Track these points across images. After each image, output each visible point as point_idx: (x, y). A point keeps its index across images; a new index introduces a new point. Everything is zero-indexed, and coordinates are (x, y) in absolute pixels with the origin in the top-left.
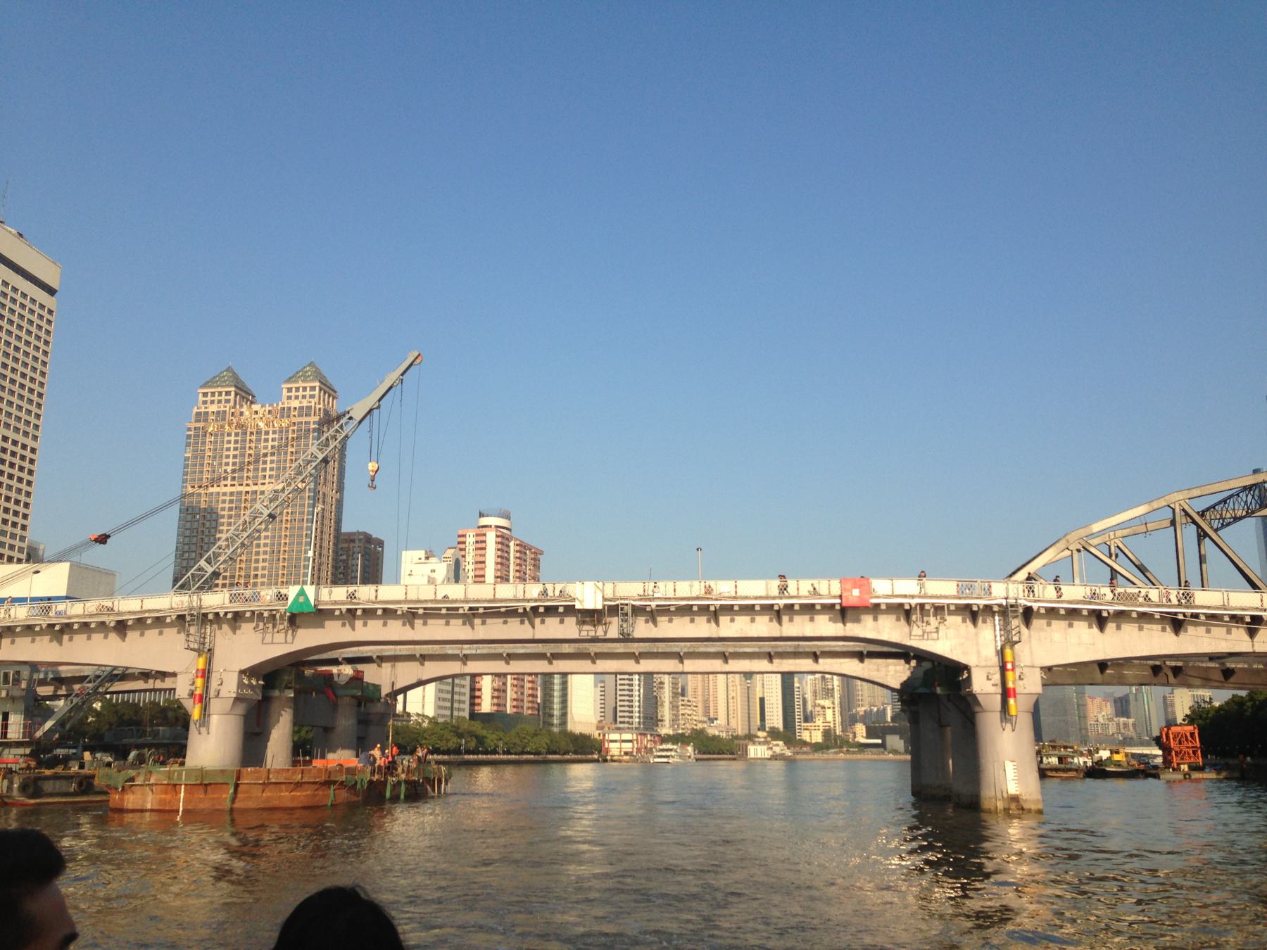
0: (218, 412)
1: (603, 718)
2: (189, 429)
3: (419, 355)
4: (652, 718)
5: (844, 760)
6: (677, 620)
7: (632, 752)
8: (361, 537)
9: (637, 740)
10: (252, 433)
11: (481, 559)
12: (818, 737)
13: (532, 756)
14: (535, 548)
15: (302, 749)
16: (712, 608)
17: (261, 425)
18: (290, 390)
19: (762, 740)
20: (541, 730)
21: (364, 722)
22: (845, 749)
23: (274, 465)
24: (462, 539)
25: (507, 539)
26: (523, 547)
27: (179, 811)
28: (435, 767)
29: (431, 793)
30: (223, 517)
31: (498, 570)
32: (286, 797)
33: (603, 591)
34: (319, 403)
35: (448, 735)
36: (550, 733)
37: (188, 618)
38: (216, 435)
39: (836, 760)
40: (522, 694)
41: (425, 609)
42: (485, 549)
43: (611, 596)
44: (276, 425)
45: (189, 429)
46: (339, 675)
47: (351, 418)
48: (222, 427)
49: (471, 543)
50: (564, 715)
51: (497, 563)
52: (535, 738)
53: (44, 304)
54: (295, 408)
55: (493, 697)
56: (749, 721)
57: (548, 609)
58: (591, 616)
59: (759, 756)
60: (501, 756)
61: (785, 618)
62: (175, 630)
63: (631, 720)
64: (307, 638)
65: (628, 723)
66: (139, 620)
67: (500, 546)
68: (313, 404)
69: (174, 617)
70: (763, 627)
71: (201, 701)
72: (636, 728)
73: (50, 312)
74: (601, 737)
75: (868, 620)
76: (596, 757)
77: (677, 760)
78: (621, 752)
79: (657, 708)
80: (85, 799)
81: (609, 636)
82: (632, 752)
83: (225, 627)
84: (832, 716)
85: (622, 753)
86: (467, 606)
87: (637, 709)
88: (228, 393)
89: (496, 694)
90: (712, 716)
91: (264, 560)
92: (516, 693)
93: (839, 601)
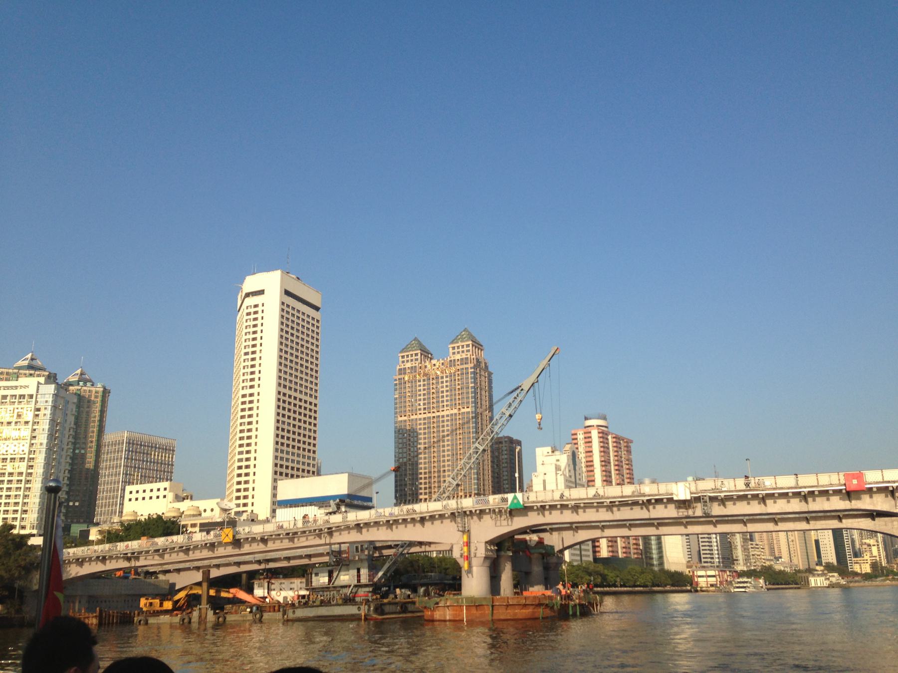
0: (412, 367)
1: (690, 559)
2: (396, 380)
3: (558, 349)
4: (729, 559)
5: (892, 585)
6: (738, 504)
7: (716, 584)
8: (506, 440)
9: (719, 575)
10: (433, 379)
11: (589, 449)
12: (867, 569)
13: (642, 588)
14: (626, 439)
15: (520, 584)
16: (761, 496)
17: (439, 373)
18: (454, 348)
19: (821, 572)
20: (645, 569)
21: (546, 568)
22: (891, 577)
23: (449, 398)
24: (574, 437)
25: (606, 434)
26: (618, 439)
27: (463, 621)
28: (593, 595)
29: (593, 612)
30: (421, 434)
31: (602, 456)
32: (510, 613)
33: (690, 488)
34: (473, 355)
35: (581, 574)
36: (653, 571)
37: (457, 514)
38: (412, 382)
39: (883, 586)
40: (629, 543)
41: (584, 503)
42: (591, 442)
43: (695, 491)
44: (447, 372)
45: (396, 380)
46: (530, 541)
47: (522, 390)
48: (415, 376)
49: (581, 439)
50: (661, 558)
51: (601, 452)
52: (643, 575)
53: (309, 314)
54: (458, 360)
55: (608, 546)
56: (808, 559)
57: (657, 500)
58: (683, 504)
59: (819, 585)
60: (620, 589)
61: (810, 500)
62: (449, 520)
63: (712, 560)
64: (520, 522)
65: (710, 562)
66: (431, 516)
67: (601, 440)
68: (469, 356)
69: (449, 514)
70: (796, 505)
71: (467, 559)
72: (717, 567)
73: (318, 321)
74: (691, 574)
75: (866, 498)
76: (689, 588)
77: (752, 589)
78: (707, 584)
79: (731, 551)
80: (404, 615)
81: (696, 515)
82: (716, 584)
83: (475, 518)
84: (877, 552)
85: (709, 585)
86: (608, 501)
87: (716, 552)
88: (416, 355)
89: (610, 544)
90: (777, 556)
91: (448, 461)
92: (624, 542)
93: (844, 487)
